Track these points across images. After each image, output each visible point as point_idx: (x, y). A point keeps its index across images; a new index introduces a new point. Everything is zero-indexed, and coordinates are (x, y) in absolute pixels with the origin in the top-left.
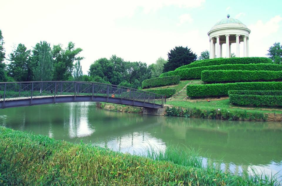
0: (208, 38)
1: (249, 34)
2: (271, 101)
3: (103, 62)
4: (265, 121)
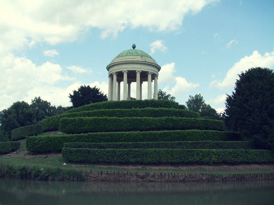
0: (107, 73)
1: (159, 71)
2: (109, 156)
3: (19, 108)
4: (83, 180)
